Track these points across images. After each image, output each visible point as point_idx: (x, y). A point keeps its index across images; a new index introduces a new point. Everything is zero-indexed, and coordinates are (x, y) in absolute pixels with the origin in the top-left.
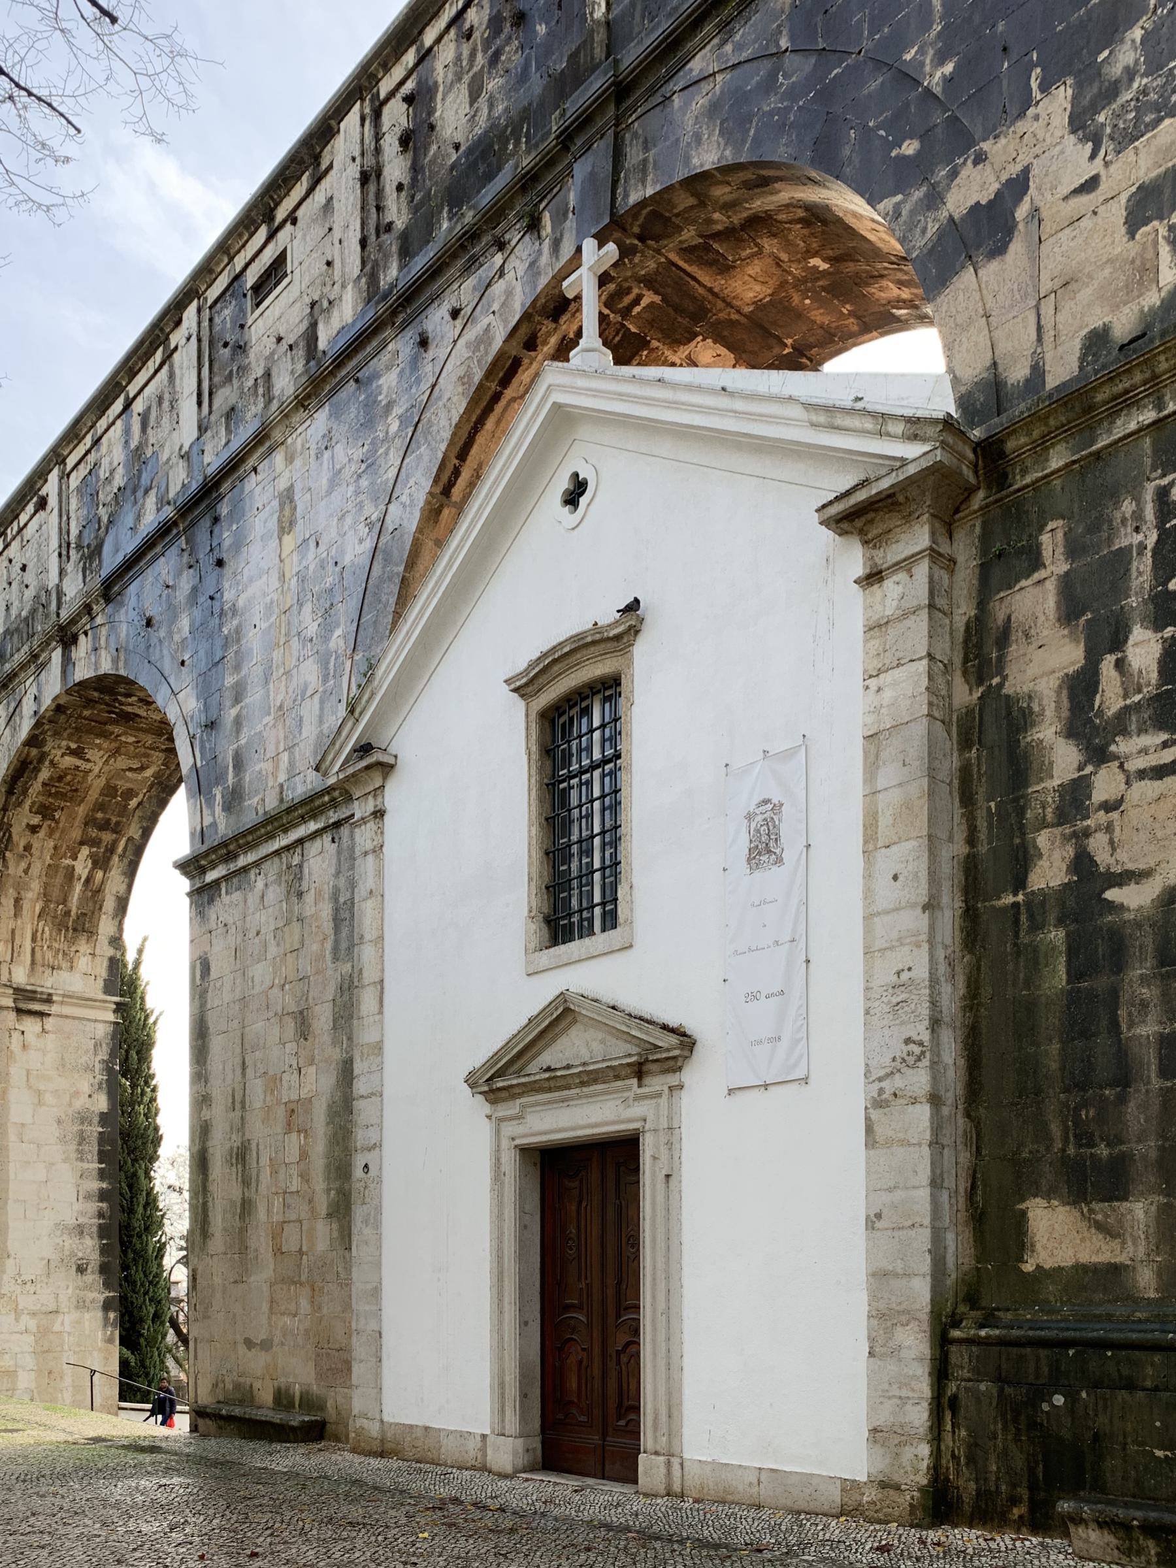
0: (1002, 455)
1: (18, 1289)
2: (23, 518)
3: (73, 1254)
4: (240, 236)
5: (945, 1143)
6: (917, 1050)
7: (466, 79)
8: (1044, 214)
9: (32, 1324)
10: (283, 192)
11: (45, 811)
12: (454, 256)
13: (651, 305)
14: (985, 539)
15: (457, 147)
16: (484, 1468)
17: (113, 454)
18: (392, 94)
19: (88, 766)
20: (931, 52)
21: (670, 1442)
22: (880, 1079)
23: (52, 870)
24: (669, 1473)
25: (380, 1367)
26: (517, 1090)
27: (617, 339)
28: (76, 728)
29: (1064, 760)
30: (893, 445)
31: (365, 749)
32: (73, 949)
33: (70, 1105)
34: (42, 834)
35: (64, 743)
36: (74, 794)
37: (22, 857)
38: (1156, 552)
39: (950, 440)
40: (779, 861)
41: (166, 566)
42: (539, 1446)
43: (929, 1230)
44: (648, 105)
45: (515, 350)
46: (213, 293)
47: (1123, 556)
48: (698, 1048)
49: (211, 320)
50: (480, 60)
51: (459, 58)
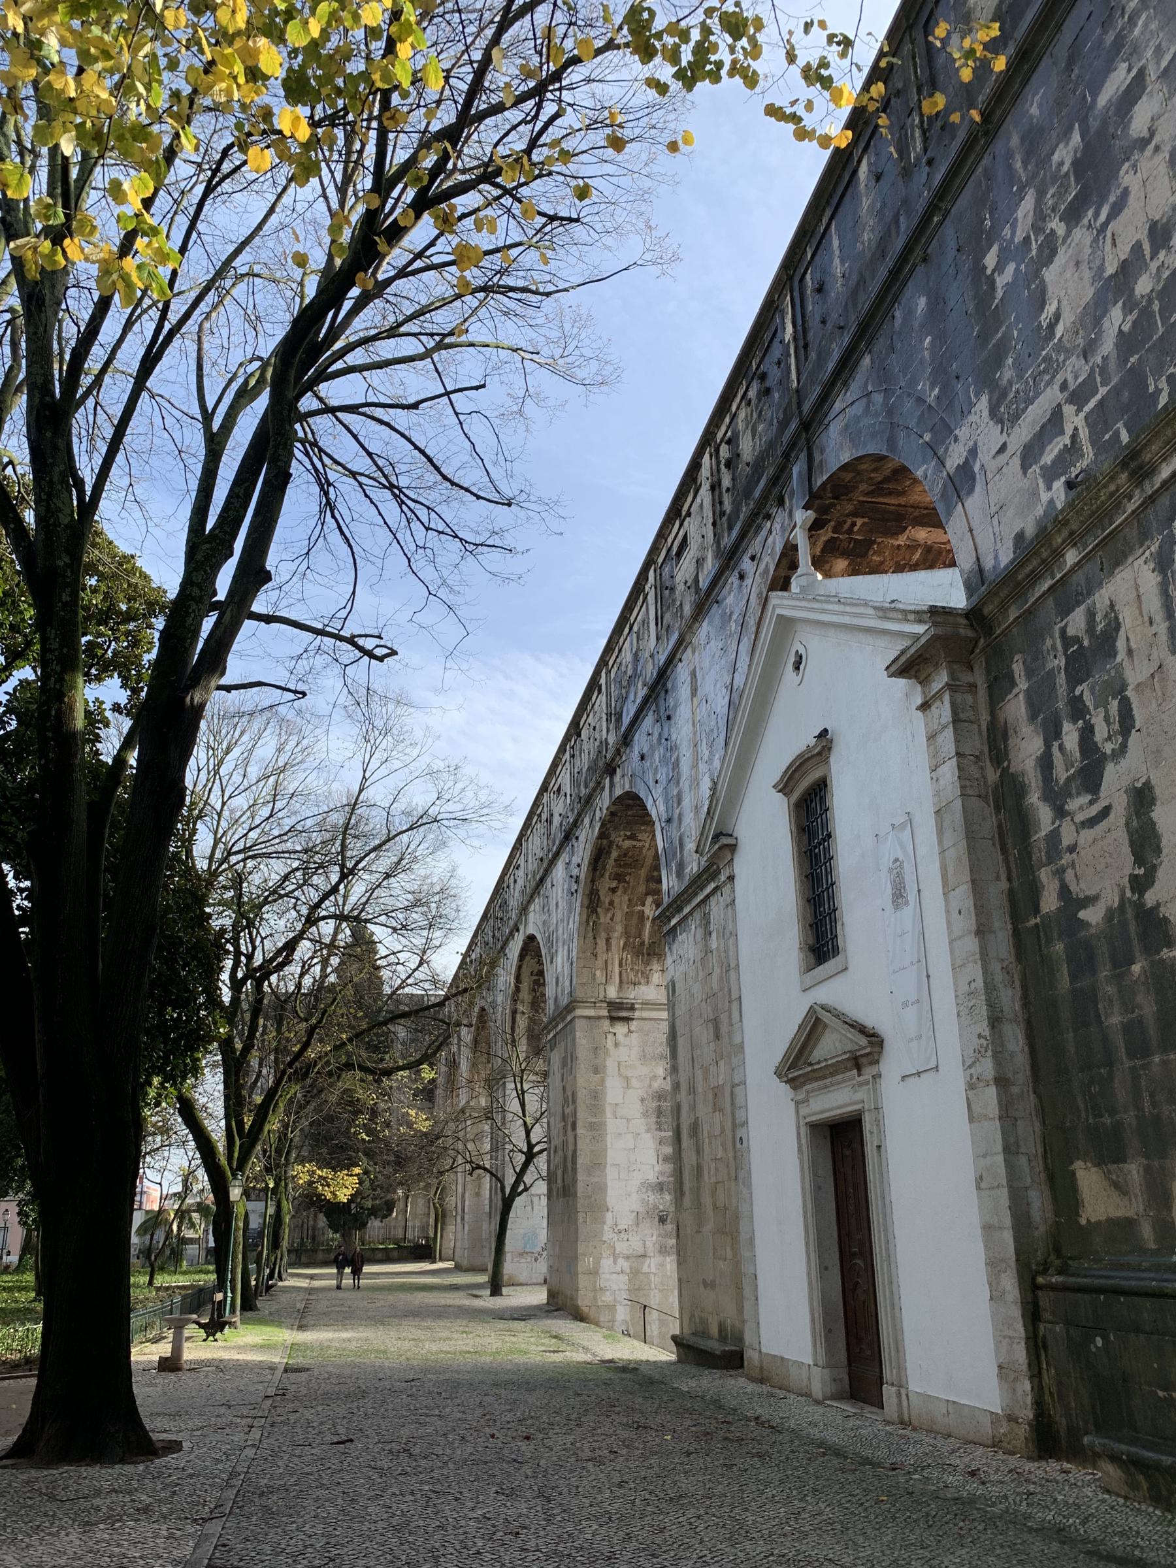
0: (984, 618)
3: (656, 1207)
11: (619, 878)
12: (750, 526)
13: (863, 524)
17: (627, 656)
21: (899, 1373)
22: (970, 1067)
23: (628, 915)
29: (1045, 815)
31: (717, 837)
33: (650, 1086)
36: (636, 863)
38: (1066, 670)
40: (907, 903)
41: (648, 722)
42: (846, 1377)
43: (1006, 1190)
45: (783, 573)
46: (660, 560)
47: (1051, 674)
50: (755, 415)
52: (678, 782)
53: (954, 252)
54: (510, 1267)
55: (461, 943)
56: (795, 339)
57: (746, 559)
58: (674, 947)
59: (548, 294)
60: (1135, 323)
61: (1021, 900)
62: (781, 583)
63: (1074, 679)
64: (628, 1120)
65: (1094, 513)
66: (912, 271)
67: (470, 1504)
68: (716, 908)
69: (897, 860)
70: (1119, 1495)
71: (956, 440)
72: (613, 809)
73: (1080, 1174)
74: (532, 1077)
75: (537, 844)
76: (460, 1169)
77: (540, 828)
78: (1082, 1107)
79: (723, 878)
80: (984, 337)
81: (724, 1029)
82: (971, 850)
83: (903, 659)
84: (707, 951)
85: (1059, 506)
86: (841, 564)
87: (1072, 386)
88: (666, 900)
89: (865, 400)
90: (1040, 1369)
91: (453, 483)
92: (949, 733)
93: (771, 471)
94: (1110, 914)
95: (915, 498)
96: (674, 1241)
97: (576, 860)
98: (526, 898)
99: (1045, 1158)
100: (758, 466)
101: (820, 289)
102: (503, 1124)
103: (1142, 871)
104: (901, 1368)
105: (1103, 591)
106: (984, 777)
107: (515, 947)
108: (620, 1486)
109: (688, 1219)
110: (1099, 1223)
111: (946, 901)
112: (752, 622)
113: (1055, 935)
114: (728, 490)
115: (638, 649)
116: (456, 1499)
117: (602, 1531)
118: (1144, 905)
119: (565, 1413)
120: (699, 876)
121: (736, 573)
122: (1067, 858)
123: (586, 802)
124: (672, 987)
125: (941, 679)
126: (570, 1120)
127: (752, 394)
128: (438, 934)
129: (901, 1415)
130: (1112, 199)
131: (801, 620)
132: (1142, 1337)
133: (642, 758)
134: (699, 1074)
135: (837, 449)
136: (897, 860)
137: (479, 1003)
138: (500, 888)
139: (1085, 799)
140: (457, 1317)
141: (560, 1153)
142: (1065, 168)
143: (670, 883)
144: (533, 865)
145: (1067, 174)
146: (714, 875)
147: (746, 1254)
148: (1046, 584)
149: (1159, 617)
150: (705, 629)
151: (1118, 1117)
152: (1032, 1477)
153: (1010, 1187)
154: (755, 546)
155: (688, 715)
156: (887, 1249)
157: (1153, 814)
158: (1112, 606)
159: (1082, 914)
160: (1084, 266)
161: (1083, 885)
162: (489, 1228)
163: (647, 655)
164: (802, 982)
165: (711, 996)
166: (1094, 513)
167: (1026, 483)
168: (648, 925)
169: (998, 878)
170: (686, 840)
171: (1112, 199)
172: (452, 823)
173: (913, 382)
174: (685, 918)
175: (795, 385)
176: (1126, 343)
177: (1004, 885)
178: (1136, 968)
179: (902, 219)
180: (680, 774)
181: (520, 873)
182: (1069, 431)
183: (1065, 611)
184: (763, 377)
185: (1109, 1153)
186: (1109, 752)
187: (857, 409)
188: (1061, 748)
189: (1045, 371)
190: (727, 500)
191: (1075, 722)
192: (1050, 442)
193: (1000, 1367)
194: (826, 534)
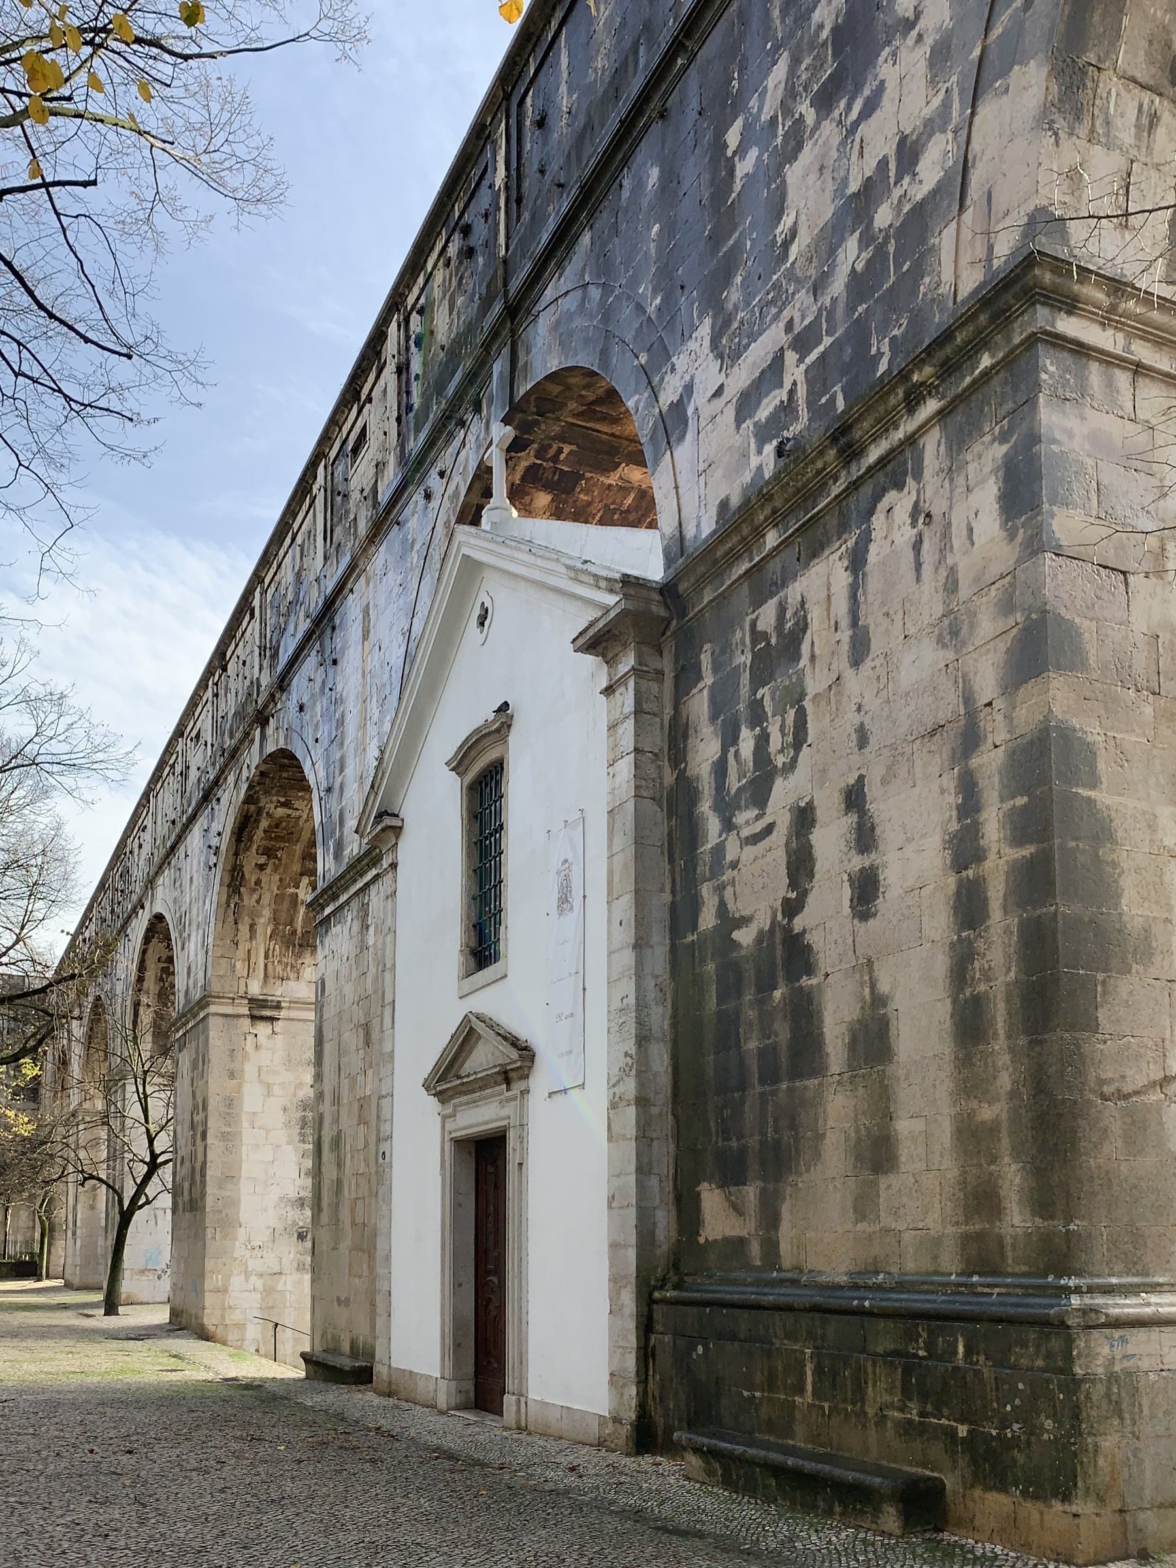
0: (679, 596)
1: (248, 1254)
3: (295, 1223)
4: (343, 412)
5: (654, 1135)
7: (447, 297)
9: (259, 1284)
10: (363, 379)
11: (268, 852)
12: (440, 432)
14: (677, 657)
15: (443, 348)
17: (287, 575)
19: (298, 813)
22: (614, 1086)
23: (279, 898)
25: (390, 1321)
26: (450, 1093)
27: (556, 477)
29: (713, 824)
31: (380, 816)
32: (300, 962)
33: (295, 1095)
34: (268, 870)
35: (275, 798)
37: (254, 890)
40: (571, 909)
41: (310, 663)
45: (475, 499)
46: (333, 454)
49: (332, 474)
50: (454, 283)
51: (444, 281)
52: (342, 744)
53: (694, 115)
54: (127, 1286)
55: (71, 919)
56: (507, 187)
57: (434, 473)
58: (327, 941)
59: (186, 58)
60: (869, 262)
61: (682, 914)
62: (471, 515)
63: (759, 680)
64: (268, 1131)
65: (799, 491)
66: (647, 127)
67: (59, 1512)
68: (375, 898)
69: (566, 861)
70: (697, 1482)
71: (673, 369)
72: (262, 768)
73: (705, 1196)
74: (157, 1080)
75: (168, 802)
76: (71, 1178)
77: (173, 783)
78: (714, 1129)
79: (385, 864)
80: (715, 240)
81: (375, 1036)
82: (638, 857)
83: (591, 633)
84: (363, 947)
85: (767, 475)
86: (543, 499)
87: (797, 328)
88: (320, 885)
89: (579, 292)
90: (647, 1375)
91: (51, 316)
92: (630, 725)
93: (467, 364)
94: (760, 937)
95: (627, 430)
96: (309, 1259)
97: (216, 827)
98: (153, 869)
99: (675, 1180)
100: (453, 352)
101: (541, 123)
102: (123, 1129)
103: (794, 895)
104: (523, 1379)
105: (797, 584)
106: (661, 778)
107: (139, 927)
108: (222, 1491)
109: (324, 1235)
110: (716, 1241)
111: (609, 911)
112: (436, 556)
113: (709, 955)
114: (417, 377)
115: (301, 568)
116: (45, 1509)
117: (198, 1530)
118: (792, 930)
119: (174, 1427)
120: (359, 860)
121: (421, 490)
122: (728, 875)
123: (233, 755)
124: (321, 985)
125: (628, 662)
126: (200, 1129)
127: (452, 251)
128: (40, 904)
129: (518, 1421)
130: (867, 92)
131: (490, 566)
132: (737, 1344)
133: (301, 708)
134: (345, 1083)
135: (545, 353)
136: (566, 861)
137: (93, 991)
138: (121, 853)
139: (751, 813)
140: (63, 1337)
141: (187, 1164)
142: (825, 34)
143: (326, 865)
144: (163, 829)
145: (825, 43)
146: (375, 861)
147: (381, 1271)
148: (745, 566)
149: (845, 622)
150: (382, 556)
151: (743, 1141)
152: (626, 1470)
153: (640, 1208)
154: (445, 460)
155: (358, 663)
156: (520, 1266)
157: (811, 837)
158: (803, 603)
159: (736, 935)
160: (827, 173)
161: (739, 904)
162: (105, 1244)
163: (312, 578)
164: (460, 988)
165: (363, 999)
166: (799, 491)
167: (737, 440)
168: (302, 910)
169: (662, 890)
170: (347, 816)
171: (867, 92)
172: (56, 768)
173: (634, 282)
174: (341, 907)
175: (503, 252)
176: (859, 285)
177: (667, 897)
178: (777, 994)
179: (642, 49)
180: (345, 730)
181: (147, 837)
182: (787, 385)
183: (758, 602)
184: (466, 231)
185: (731, 1174)
186: (780, 765)
187: (570, 303)
188: (737, 754)
189: (773, 302)
190: (416, 389)
191: (753, 729)
192: (767, 395)
193: (612, 1374)
194: (527, 459)
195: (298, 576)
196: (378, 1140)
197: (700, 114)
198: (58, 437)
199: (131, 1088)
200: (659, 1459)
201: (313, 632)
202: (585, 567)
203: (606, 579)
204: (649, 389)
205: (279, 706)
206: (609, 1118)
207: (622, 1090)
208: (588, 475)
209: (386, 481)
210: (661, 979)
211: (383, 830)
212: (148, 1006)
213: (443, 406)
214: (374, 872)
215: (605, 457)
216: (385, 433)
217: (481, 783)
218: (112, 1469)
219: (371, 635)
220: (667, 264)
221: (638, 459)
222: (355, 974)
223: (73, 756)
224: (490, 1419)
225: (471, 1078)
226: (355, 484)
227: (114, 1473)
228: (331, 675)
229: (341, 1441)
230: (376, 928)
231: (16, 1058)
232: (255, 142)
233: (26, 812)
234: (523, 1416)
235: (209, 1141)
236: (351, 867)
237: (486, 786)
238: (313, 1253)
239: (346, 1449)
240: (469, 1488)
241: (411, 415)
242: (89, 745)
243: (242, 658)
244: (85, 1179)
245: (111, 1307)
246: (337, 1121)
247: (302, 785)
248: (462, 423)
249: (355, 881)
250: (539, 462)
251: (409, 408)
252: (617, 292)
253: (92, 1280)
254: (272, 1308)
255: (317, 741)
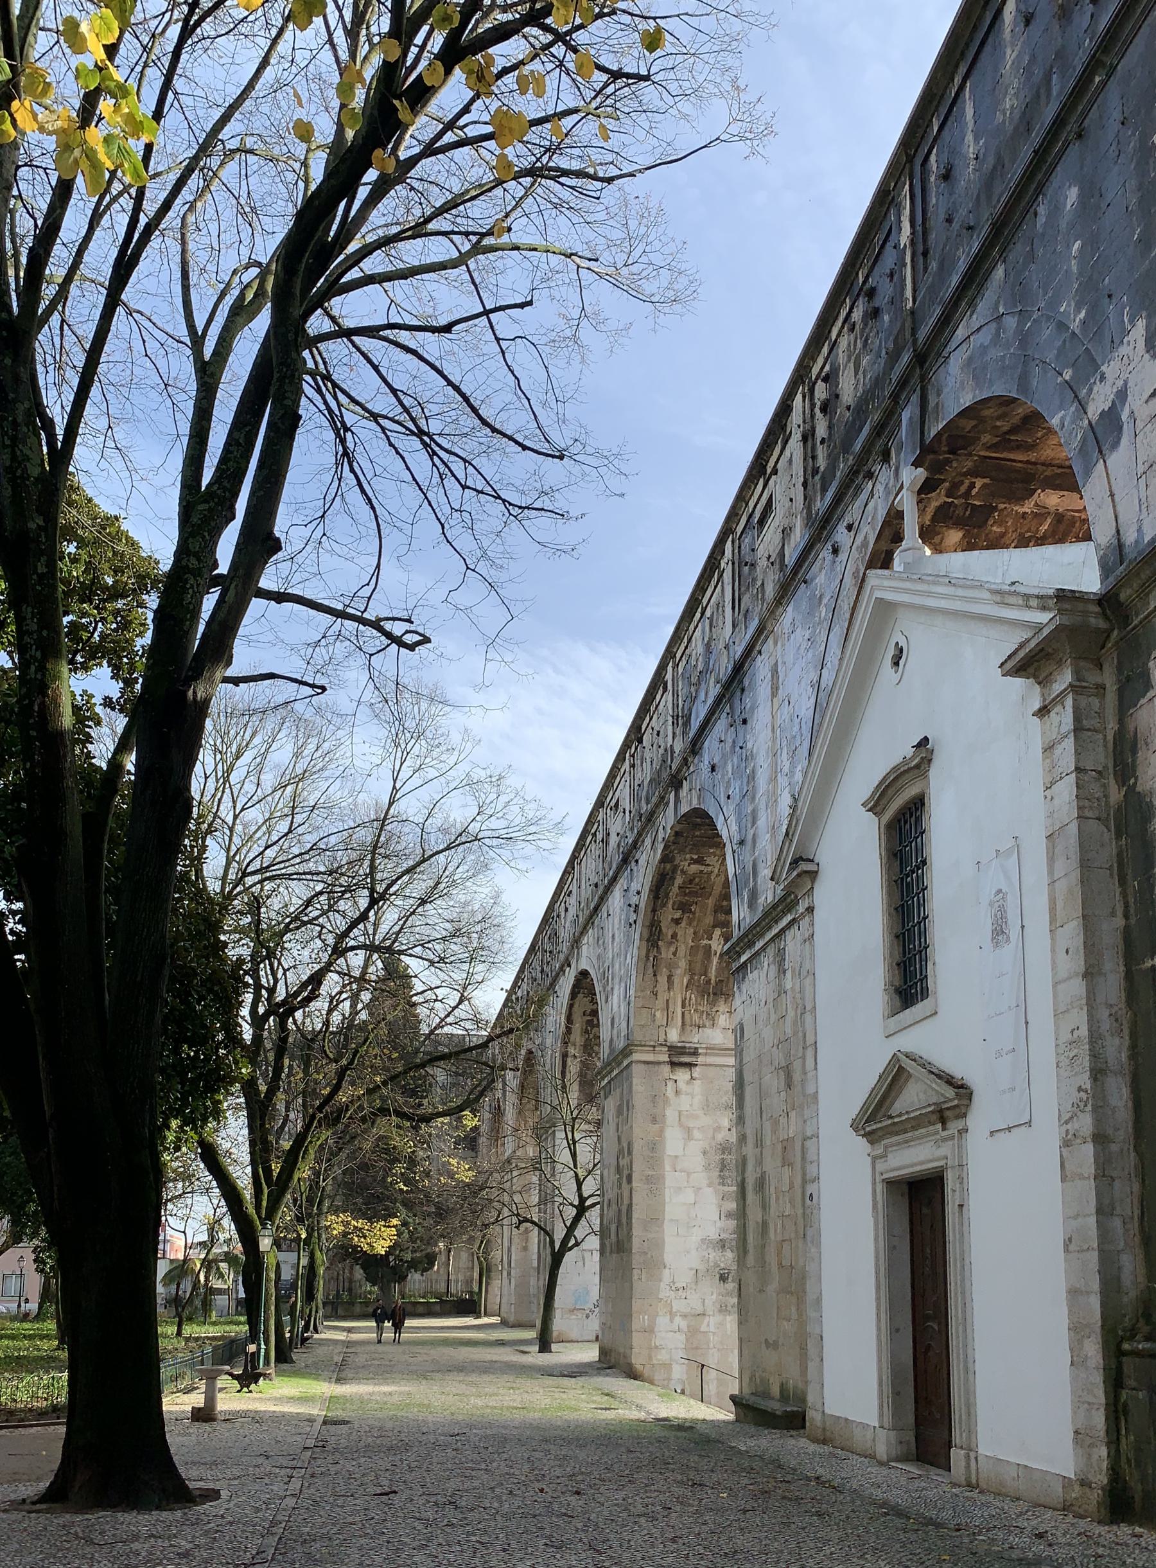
0: (1121, 604)
2: (658, 697)
6: (1084, 1096)
8: (1136, 414)
9: (683, 1324)
11: (683, 907)
12: (848, 487)
13: (984, 486)
14: (1120, 668)
16: (872, 1456)
17: (698, 647)
18: (817, 379)
20: (1073, 304)
21: (969, 1438)
22: (1066, 1122)
23: (693, 950)
24: (968, 1466)
27: (968, 513)
28: (694, 845)
30: (1034, 614)
31: (796, 862)
32: (714, 1010)
34: (683, 924)
35: (688, 856)
37: (671, 943)
39: (1067, 606)
40: (1008, 940)
41: (721, 726)
43: (1097, 1253)
44: (938, 364)
45: (884, 546)
48: (975, 1098)
49: (740, 547)
52: (753, 798)
53: (1117, 126)
54: (558, 1324)
55: (506, 978)
57: (841, 528)
58: (744, 987)
59: (610, 180)
62: (882, 559)
64: (689, 1174)
68: (792, 943)
69: (999, 891)
71: (1103, 378)
74: (584, 1127)
75: (590, 868)
77: (595, 850)
79: (801, 909)
81: (797, 1077)
82: (1084, 881)
83: (1021, 654)
84: (781, 991)
86: (954, 536)
89: (994, 325)
91: (494, 430)
92: (1069, 744)
95: (1047, 453)
97: (635, 886)
100: (860, 410)
102: (553, 1175)
104: (971, 1431)
108: (674, 1540)
109: (751, 1278)
120: (774, 907)
123: (649, 819)
124: (739, 1032)
125: (1064, 678)
126: (625, 1173)
127: (857, 316)
128: (480, 968)
133: (713, 769)
134: (768, 1126)
135: (957, 389)
137: (526, 1045)
140: (503, 1372)
141: (614, 1207)
143: (741, 915)
144: (586, 892)
147: (812, 1314)
150: (789, 615)
153: (1101, 1251)
154: (852, 514)
163: (721, 646)
164: (885, 1027)
168: (715, 960)
169: (1113, 914)
170: (761, 866)
172: (495, 842)
173: (1054, 304)
174: (757, 954)
175: (910, 304)
177: (1120, 921)
181: (572, 900)
184: (871, 293)
190: (821, 452)
193: (1076, 1432)
194: (938, 499)
195: (708, 646)
196: (804, 1182)
197: (1123, 123)
198: (498, 540)
199: (560, 1135)
200: (1138, 1530)
201: (724, 696)
202: (1013, 589)
203: (1037, 597)
204: (1076, 404)
205: (692, 769)
206: (1061, 1156)
207: (1076, 1126)
208: (1001, 506)
209: (793, 544)
210: (1116, 1008)
211: (799, 875)
212: (575, 1057)
213: (850, 462)
214: (789, 917)
215: (1020, 485)
216: (791, 500)
217: (899, 821)
218: (563, 1511)
219: (780, 692)
220: (1090, 278)
221: (1066, 480)
222: (773, 1017)
223: (510, 830)
224: (935, 1474)
225: (904, 1118)
226: (761, 552)
227: (565, 1514)
228: (740, 735)
229: (784, 1493)
230: (793, 971)
231: (461, 1109)
232: (672, 248)
233: (468, 884)
234: (973, 1472)
235: (634, 1184)
236: (766, 915)
237: (906, 822)
238: (740, 1296)
239: (790, 1500)
240: (929, 1551)
241: (817, 478)
242: (524, 820)
243: (657, 729)
244: (520, 1222)
245: (545, 1344)
246: (761, 1163)
247: (714, 840)
248: (870, 475)
249: (770, 928)
250: (950, 500)
251: (815, 471)
252: (1035, 317)
253: (525, 1318)
254: (697, 1348)
255: (729, 797)
